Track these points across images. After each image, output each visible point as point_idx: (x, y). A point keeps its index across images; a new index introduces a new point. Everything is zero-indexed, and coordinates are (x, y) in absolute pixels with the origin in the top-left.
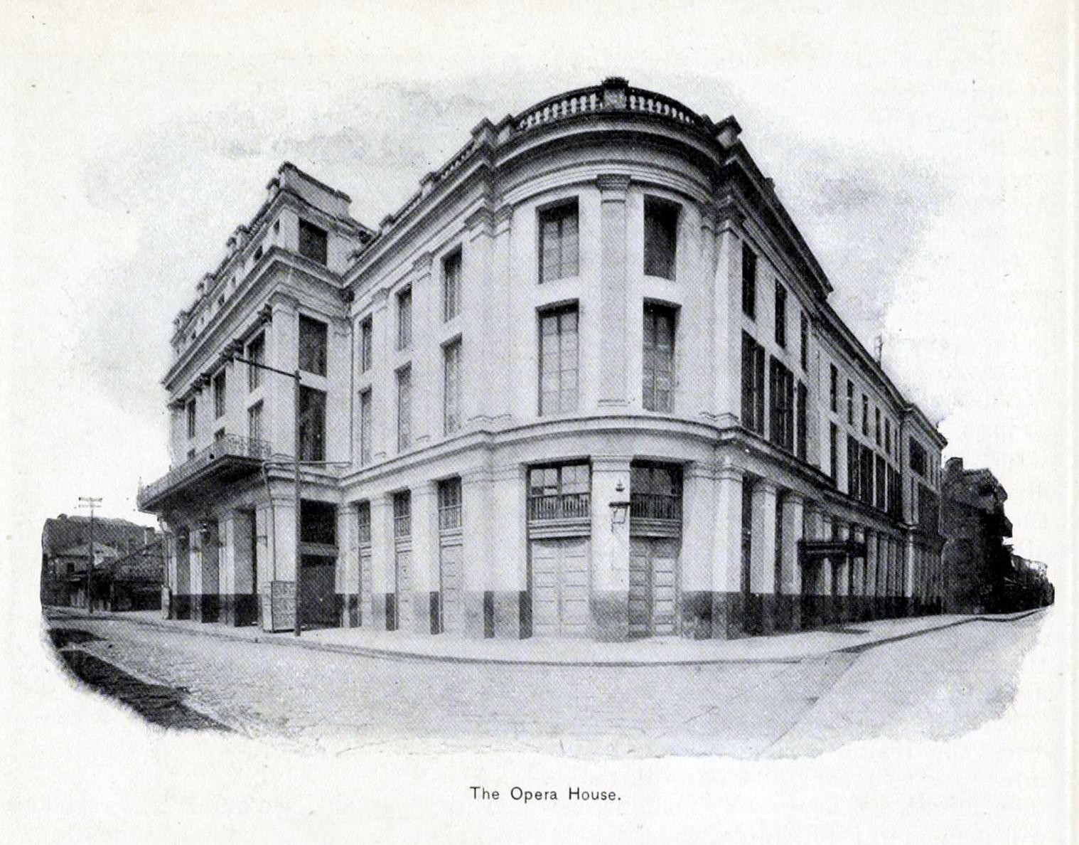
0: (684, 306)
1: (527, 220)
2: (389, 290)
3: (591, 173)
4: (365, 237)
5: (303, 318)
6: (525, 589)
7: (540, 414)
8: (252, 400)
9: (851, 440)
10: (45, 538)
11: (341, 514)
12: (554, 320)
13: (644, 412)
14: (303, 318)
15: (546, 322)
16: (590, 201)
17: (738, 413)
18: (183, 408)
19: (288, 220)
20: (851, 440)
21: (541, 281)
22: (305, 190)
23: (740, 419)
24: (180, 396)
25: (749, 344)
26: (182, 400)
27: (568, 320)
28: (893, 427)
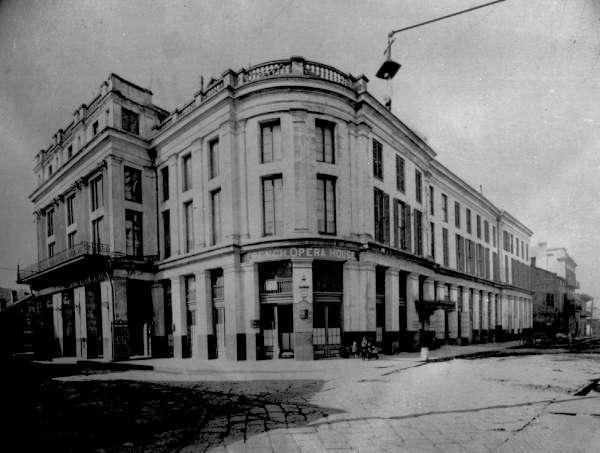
0: (340, 178)
1: (253, 127)
2: (203, 138)
3: (287, 106)
4: (162, 115)
5: (127, 169)
6: (211, 332)
7: (265, 235)
8: (93, 216)
9: (458, 237)
10: (91, 372)
11: (348, 269)
12: (270, 182)
13: (319, 236)
14: (127, 169)
15: (266, 182)
16: (287, 120)
17: (372, 233)
18: (86, 185)
19: (113, 106)
20: (458, 237)
21: (262, 161)
22: (124, 90)
23: (373, 236)
24: (42, 206)
25: (378, 193)
26: (43, 212)
27: (277, 181)
28: (491, 225)
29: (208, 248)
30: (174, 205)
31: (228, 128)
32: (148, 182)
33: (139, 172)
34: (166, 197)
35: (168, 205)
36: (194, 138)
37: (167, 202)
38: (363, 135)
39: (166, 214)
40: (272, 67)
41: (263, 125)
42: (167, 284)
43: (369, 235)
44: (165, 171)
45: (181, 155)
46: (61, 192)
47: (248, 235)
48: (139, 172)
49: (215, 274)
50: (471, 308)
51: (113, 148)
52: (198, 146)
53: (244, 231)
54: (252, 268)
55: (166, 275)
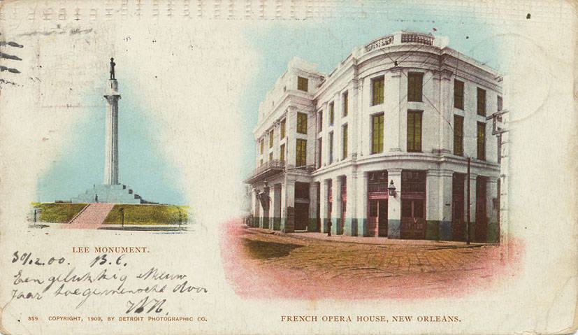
16: (388, 76)
23: (452, 152)
29: (340, 162)
30: (324, 135)
31: (352, 85)
32: (311, 122)
33: (306, 115)
34: (321, 130)
35: (321, 135)
36: (335, 92)
37: (321, 133)
38: (445, 78)
39: (320, 140)
40: (384, 40)
41: (374, 80)
42: (318, 184)
43: (449, 151)
44: (321, 113)
45: (342, 92)
46: (278, 118)
47: (362, 155)
48: (306, 115)
49: (343, 179)
50: (330, 204)
51: (291, 102)
52: (325, 106)
53: (359, 153)
54: (363, 175)
55: (317, 180)
